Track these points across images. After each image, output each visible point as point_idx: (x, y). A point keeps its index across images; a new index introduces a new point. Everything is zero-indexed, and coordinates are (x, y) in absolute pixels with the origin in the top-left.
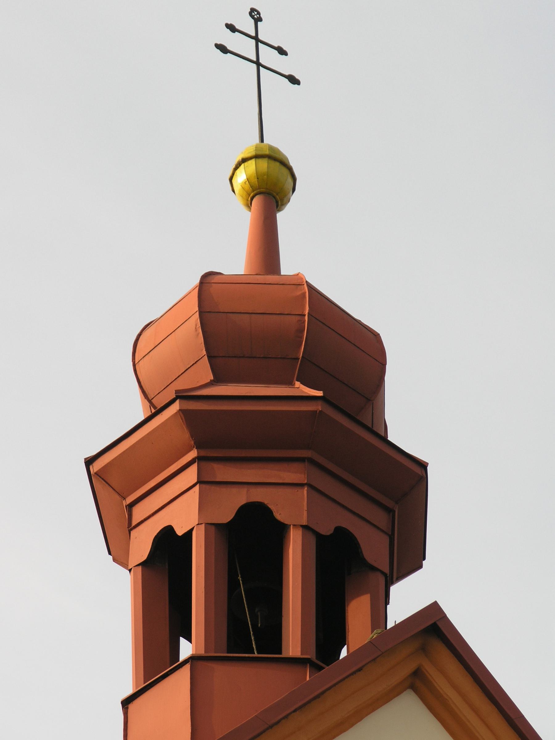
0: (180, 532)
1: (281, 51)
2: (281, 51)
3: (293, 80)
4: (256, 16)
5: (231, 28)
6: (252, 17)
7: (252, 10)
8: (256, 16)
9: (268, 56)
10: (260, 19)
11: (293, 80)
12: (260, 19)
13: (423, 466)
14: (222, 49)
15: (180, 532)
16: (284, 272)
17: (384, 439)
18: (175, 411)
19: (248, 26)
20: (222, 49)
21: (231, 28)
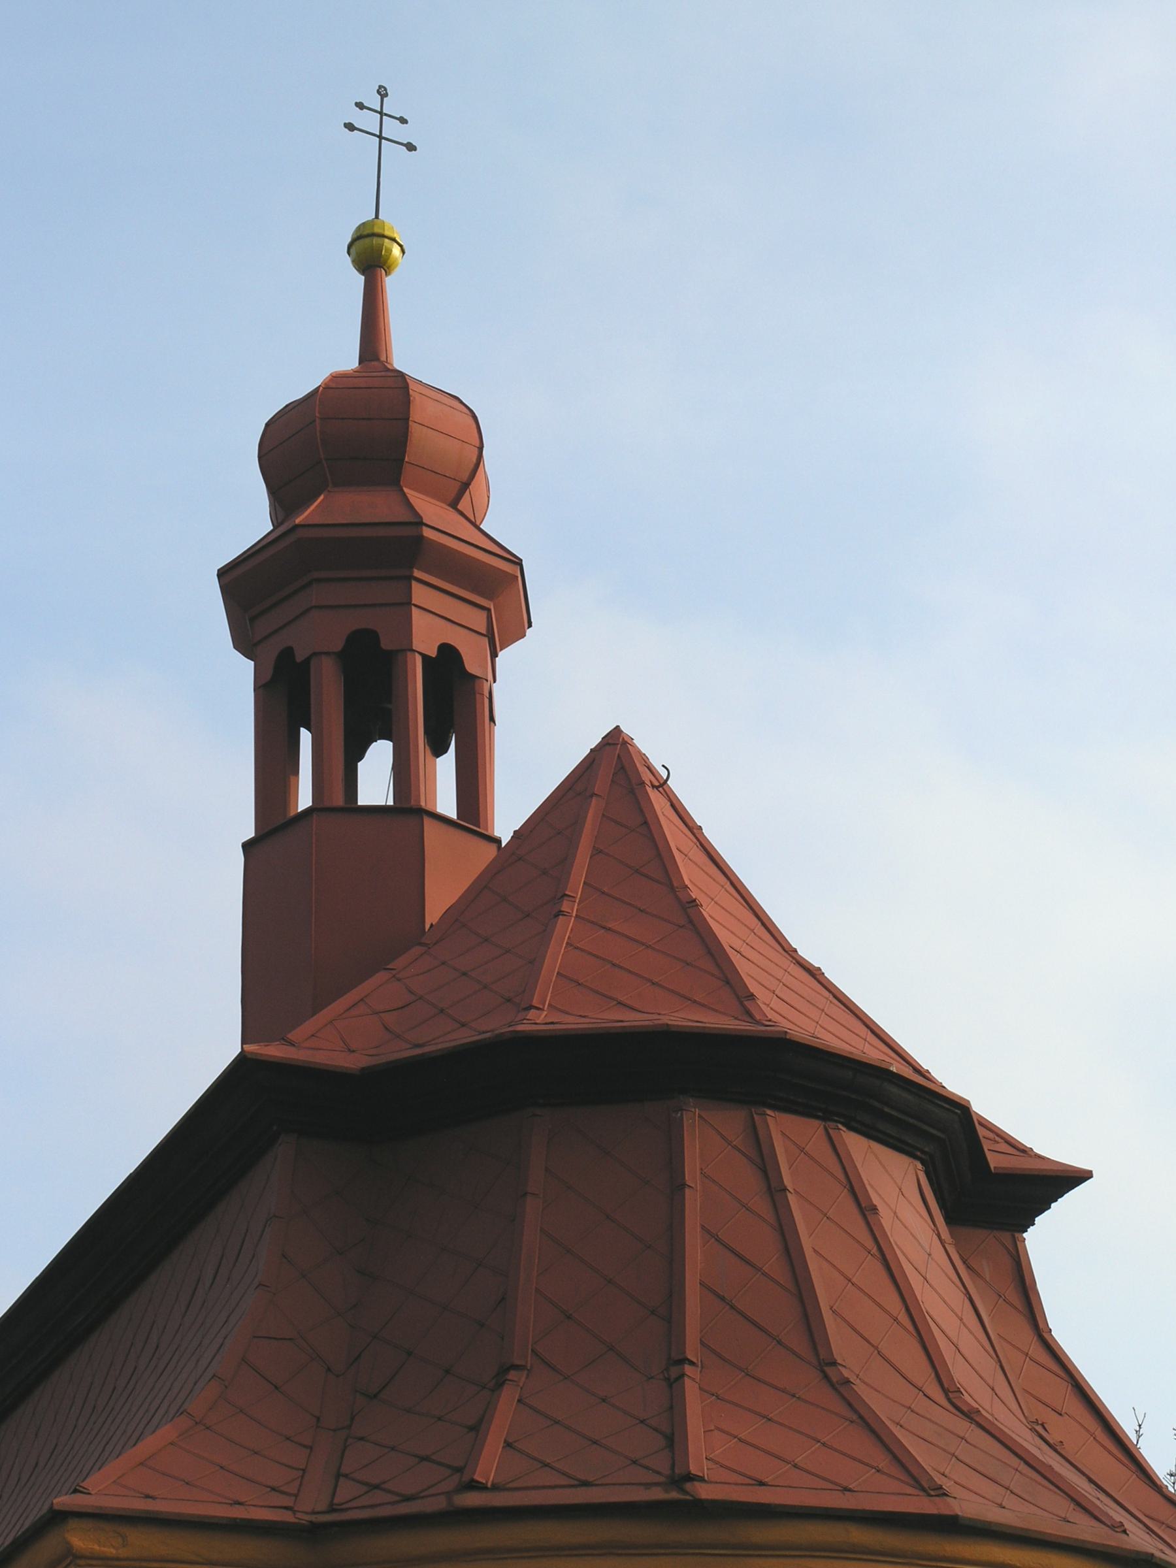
0: (300, 657)
1: (403, 121)
2: (403, 121)
3: (411, 147)
4: (382, 93)
5: (360, 106)
6: (378, 92)
7: (380, 87)
8: (382, 93)
9: (391, 128)
10: (386, 95)
11: (411, 147)
12: (386, 95)
13: (222, 573)
14: (350, 127)
15: (300, 657)
16: (360, 803)
17: (494, 655)
18: (786, 1182)
19: (374, 101)
20: (350, 127)
21: (360, 106)
